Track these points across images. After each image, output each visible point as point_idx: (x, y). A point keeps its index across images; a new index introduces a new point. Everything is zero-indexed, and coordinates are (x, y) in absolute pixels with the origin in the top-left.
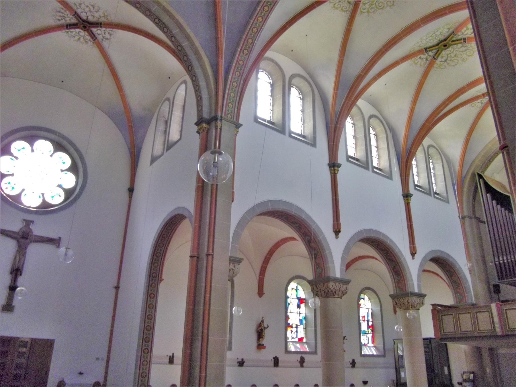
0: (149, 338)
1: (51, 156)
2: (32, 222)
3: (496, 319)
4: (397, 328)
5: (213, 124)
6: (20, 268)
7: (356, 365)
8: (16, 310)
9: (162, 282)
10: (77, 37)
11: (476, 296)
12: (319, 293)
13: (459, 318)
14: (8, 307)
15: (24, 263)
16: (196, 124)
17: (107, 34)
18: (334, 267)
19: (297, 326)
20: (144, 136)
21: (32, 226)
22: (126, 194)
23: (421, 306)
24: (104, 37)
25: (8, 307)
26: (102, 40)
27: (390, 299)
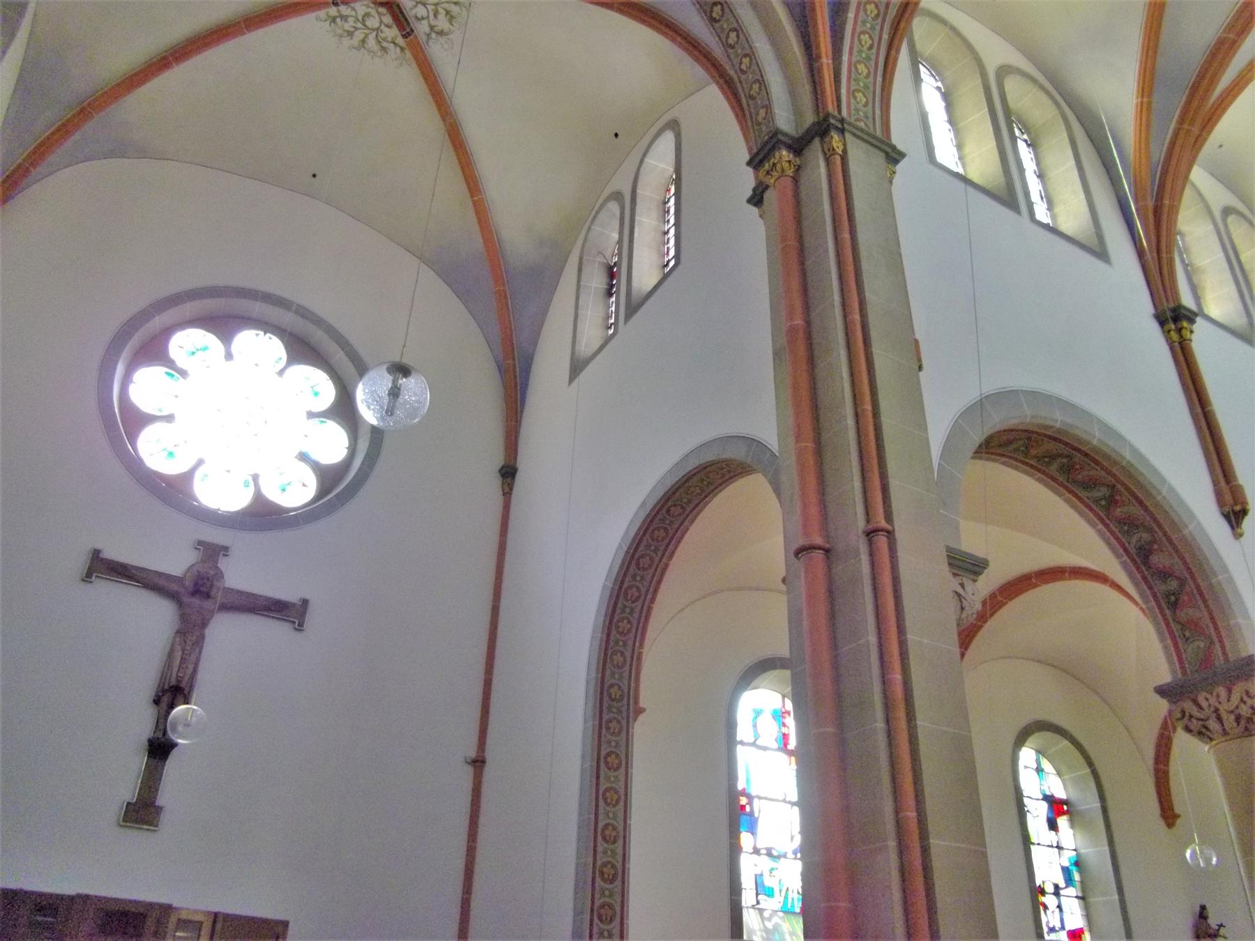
0: (611, 906)
1: (281, 373)
2: (225, 550)
5: (815, 151)
6: (183, 685)
8: (165, 818)
9: (641, 718)
10: (359, 35)
12: (1213, 724)
14: (143, 812)
15: (195, 671)
16: (749, 163)
17: (442, 15)
19: (1057, 891)
20: (544, 312)
21: (223, 564)
22: (494, 484)
24: (432, 28)
25: (143, 812)
26: (428, 35)
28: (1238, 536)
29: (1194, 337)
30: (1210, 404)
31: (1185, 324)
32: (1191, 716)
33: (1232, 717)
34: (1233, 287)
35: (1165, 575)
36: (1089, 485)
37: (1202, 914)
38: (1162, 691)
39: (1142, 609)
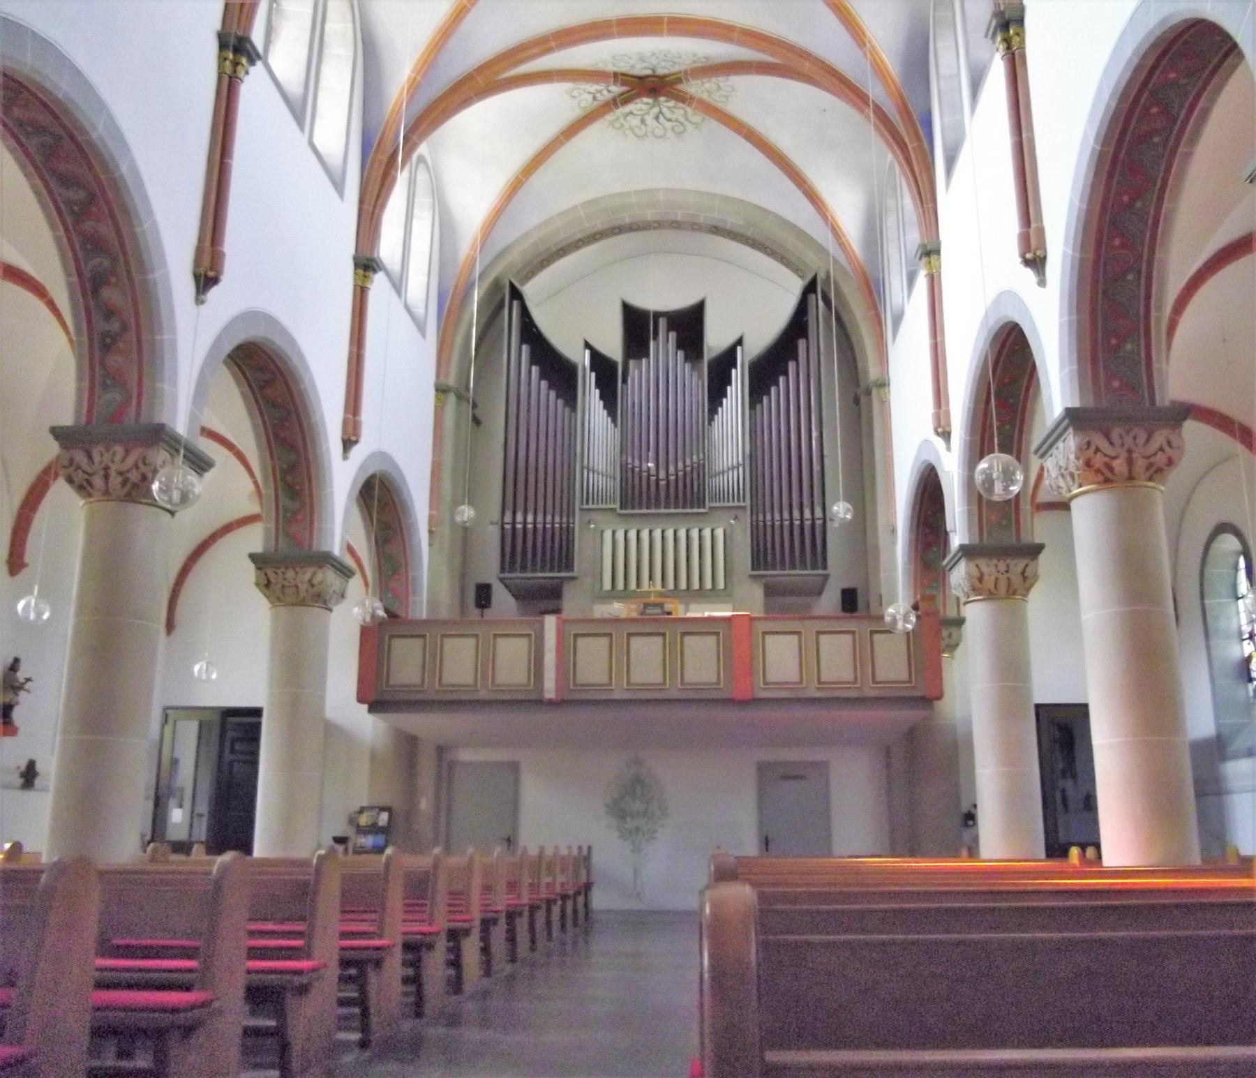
3: (550, 658)
4: (200, 671)
7: (37, 781)
11: (433, 603)
12: (98, 481)
13: (442, 646)
18: (175, 399)
23: (337, 603)
27: (251, 567)
28: (199, 300)
29: (247, 79)
30: (231, 157)
31: (244, 61)
32: (79, 467)
33: (120, 479)
34: (305, 51)
35: (110, 313)
36: (67, 181)
37: (14, 666)
38: (58, 433)
39: (71, 340)
